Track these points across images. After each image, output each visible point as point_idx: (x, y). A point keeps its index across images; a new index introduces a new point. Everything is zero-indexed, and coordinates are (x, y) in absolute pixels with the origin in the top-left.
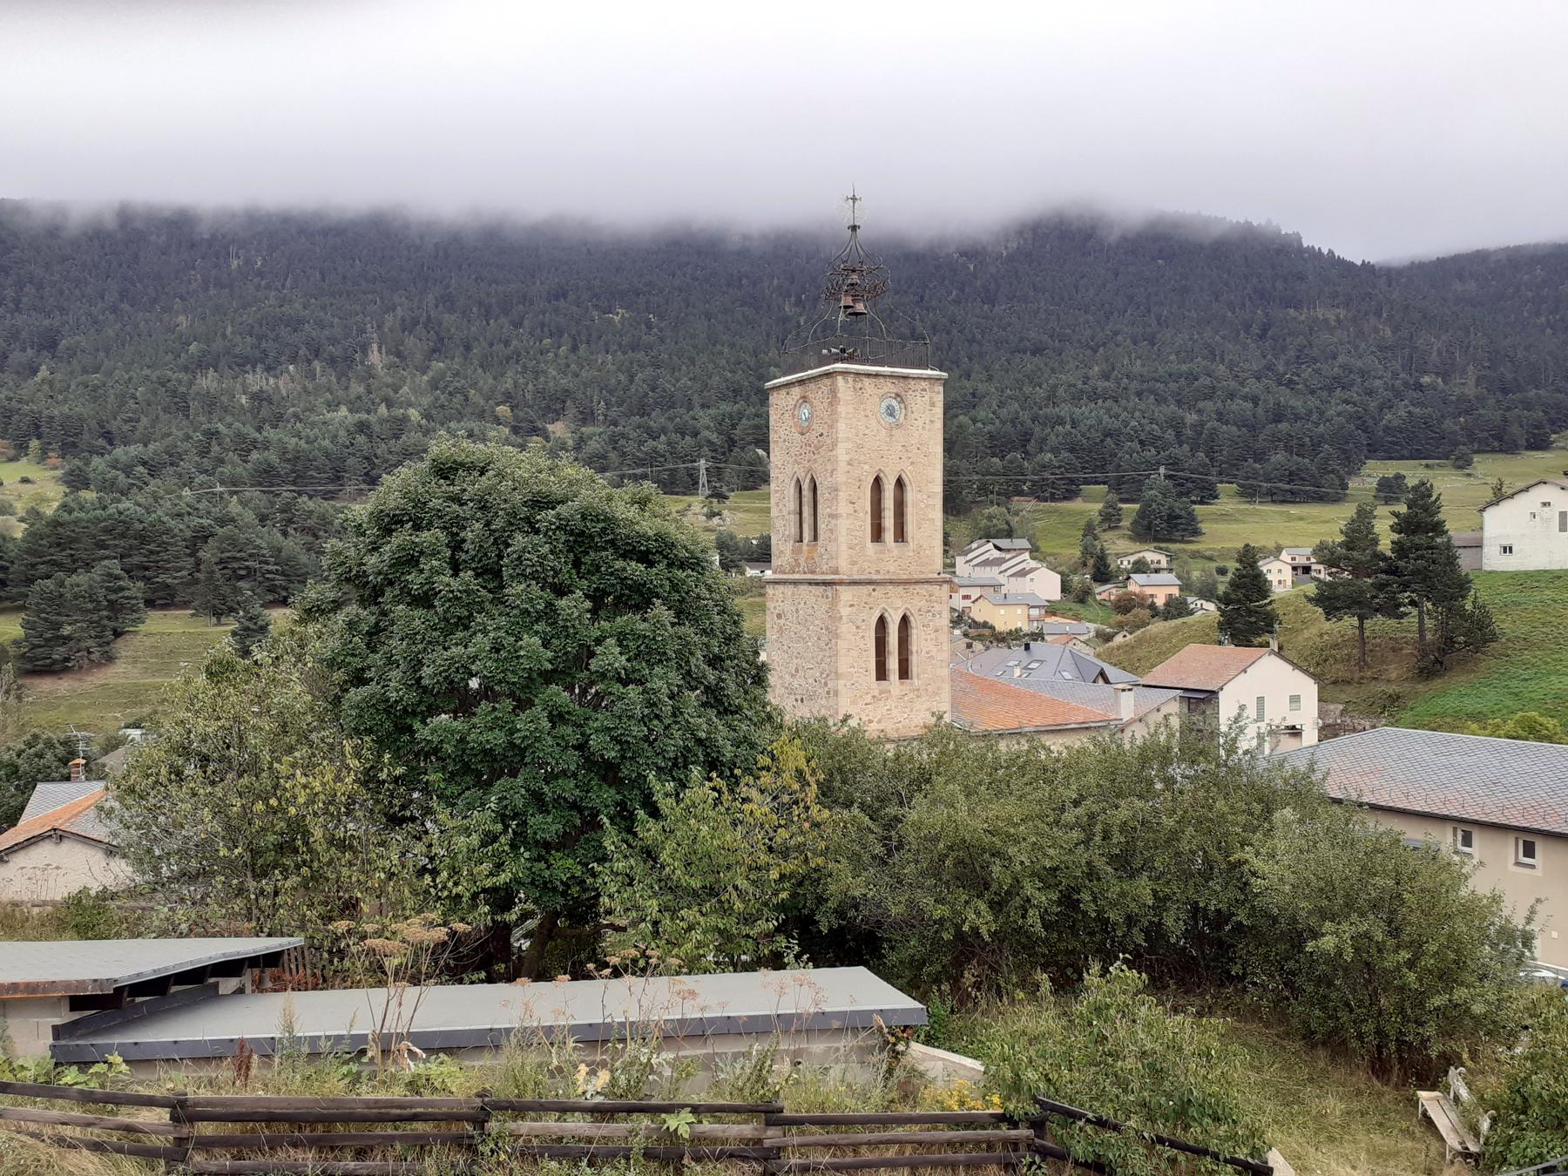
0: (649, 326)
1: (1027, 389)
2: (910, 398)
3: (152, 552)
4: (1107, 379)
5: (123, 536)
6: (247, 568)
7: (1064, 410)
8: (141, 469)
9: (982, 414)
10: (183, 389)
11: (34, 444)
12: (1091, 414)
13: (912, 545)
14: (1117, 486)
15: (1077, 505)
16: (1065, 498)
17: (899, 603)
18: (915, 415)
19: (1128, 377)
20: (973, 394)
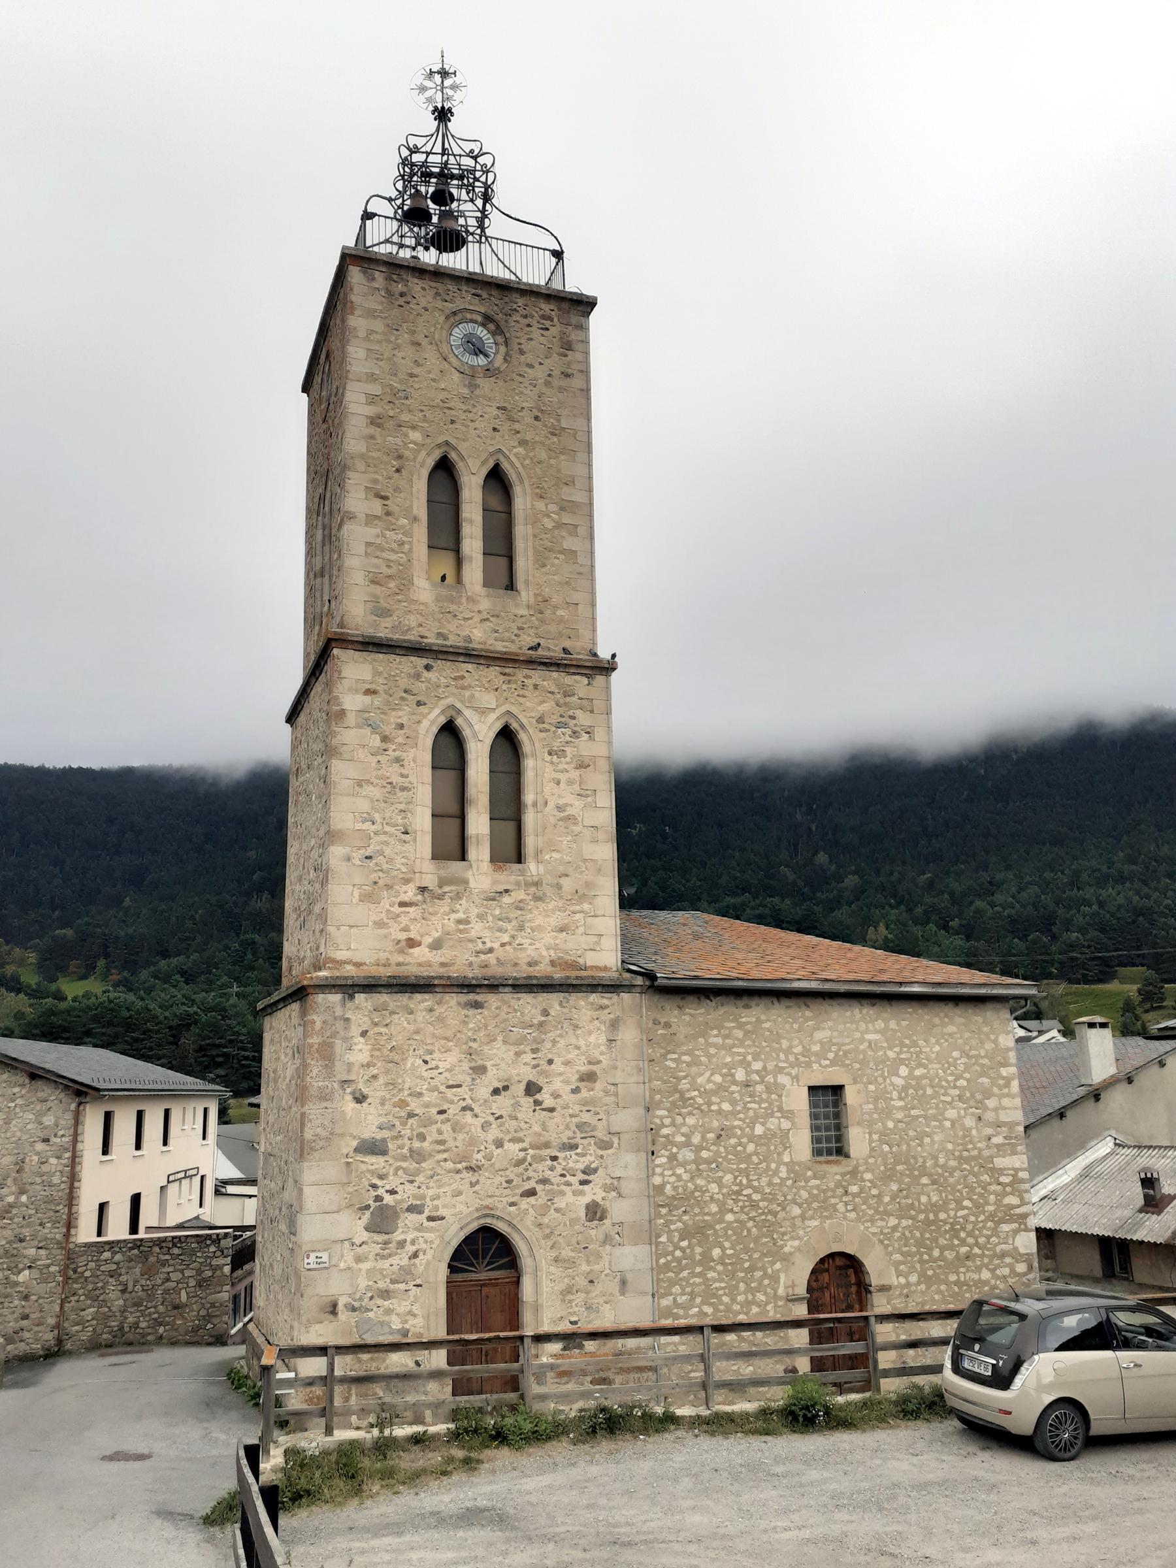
0: (664, 836)
1: (1048, 875)
2: (515, 325)
3: (136, 1040)
4: (1135, 863)
5: (110, 1024)
6: (225, 1055)
7: (1089, 893)
8: (178, 977)
9: (999, 898)
10: (237, 910)
11: (101, 963)
12: (1117, 896)
13: (525, 594)
14: (1156, 963)
15: (1113, 986)
16: (1100, 981)
17: (488, 699)
18: (529, 358)
19: (1156, 861)
20: (991, 883)
